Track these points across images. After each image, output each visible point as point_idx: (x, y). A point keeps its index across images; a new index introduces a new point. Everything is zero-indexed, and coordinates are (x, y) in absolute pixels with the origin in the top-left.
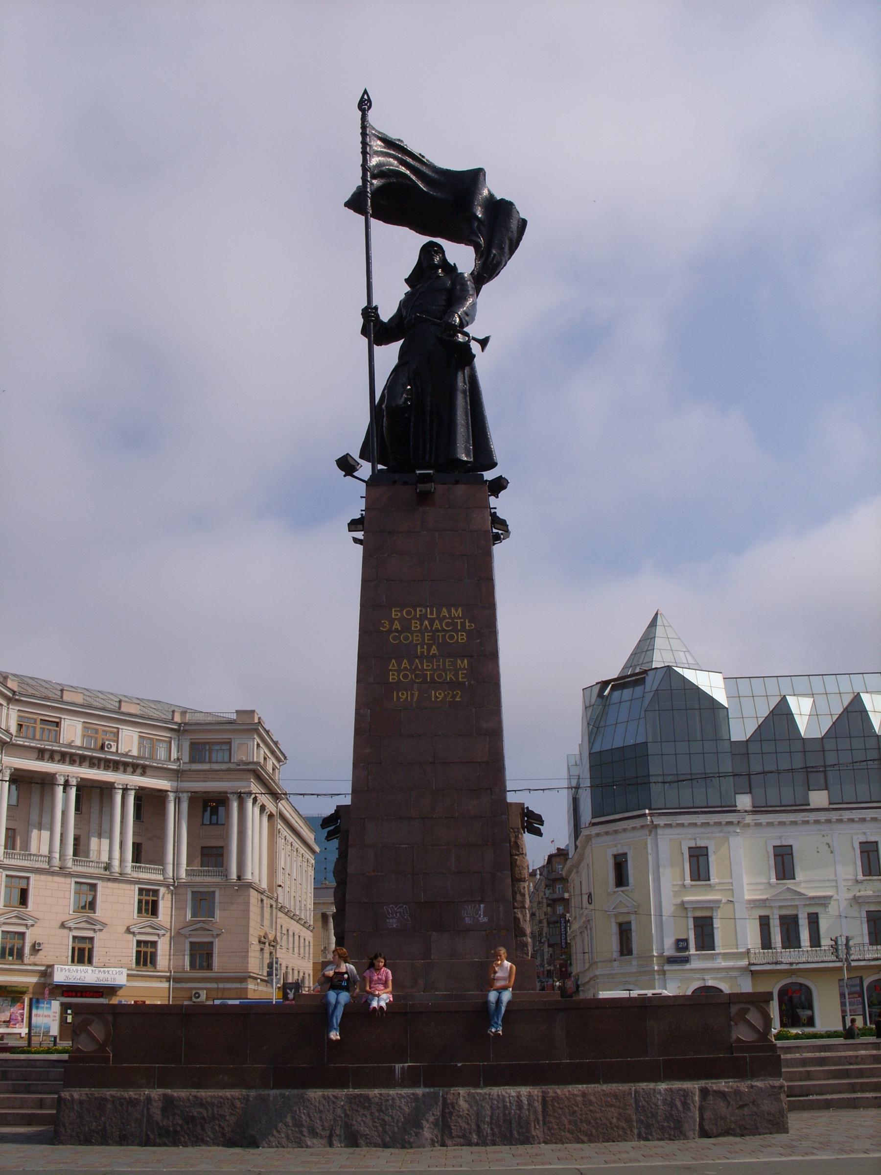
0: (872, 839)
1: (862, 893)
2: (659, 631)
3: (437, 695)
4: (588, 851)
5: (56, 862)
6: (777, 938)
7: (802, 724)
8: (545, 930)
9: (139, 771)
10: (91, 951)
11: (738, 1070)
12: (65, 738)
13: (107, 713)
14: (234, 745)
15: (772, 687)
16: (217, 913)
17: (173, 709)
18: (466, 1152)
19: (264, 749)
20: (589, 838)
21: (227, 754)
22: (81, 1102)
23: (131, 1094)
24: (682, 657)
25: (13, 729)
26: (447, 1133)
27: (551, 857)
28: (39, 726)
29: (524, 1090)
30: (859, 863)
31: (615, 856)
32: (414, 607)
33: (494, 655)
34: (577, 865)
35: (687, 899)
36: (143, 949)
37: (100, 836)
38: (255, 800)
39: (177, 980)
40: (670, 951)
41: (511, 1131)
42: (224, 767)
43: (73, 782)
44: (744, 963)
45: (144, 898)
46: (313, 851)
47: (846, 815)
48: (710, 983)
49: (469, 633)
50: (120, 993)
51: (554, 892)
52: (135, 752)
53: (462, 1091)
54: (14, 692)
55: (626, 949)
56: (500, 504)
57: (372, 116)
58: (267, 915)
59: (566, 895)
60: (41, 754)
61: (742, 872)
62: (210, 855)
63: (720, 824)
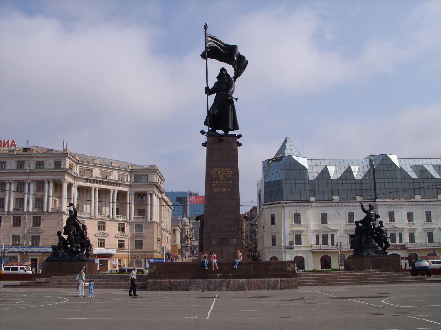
0: (352, 212)
1: (348, 228)
2: (288, 143)
3: (224, 190)
4: (263, 212)
5: (93, 215)
6: (321, 242)
8: (249, 235)
9: (118, 185)
10: (104, 243)
11: (288, 276)
12: (94, 175)
13: (108, 166)
14: (149, 176)
15: (323, 163)
16: (144, 231)
17: (129, 164)
18: (232, 292)
19: (158, 177)
20: (263, 209)
21: (146, 179)
22: (152, 282)
23: (162, 280)
24: (295, 152)
25: (78, 173)
26: (228, 288)
27: (251, 210)
28: (86, 171)
29: (244, 280)
30: (347, 219)
31: (271, 215)
32: (219, 168)
33: (238, 180)
34: (260, 216)
35: (293, 229)
36: (120, 243)
37: (105, 206)
38: (156, 194)
39: (131, 252)
40: (287, 245)
41: (241, 288)
42: (145, 184)
44: (311, 249)
45: (120, 226)
46: (171, 209)
47: (344, 204)
48: (300, 255)
49: (232, 174)
50: (113, 256)
51: (252, 222)
52: (117, 179)
53: (231, 280)
54: (78, 161)
55: (274, 244)
56: (240, 140)
57: (208, 31)
58: (159, 231)
59: (256, 223)
60: (87, 180)
61: (311, 221)
62: (141, 212)
63: (304, 206)
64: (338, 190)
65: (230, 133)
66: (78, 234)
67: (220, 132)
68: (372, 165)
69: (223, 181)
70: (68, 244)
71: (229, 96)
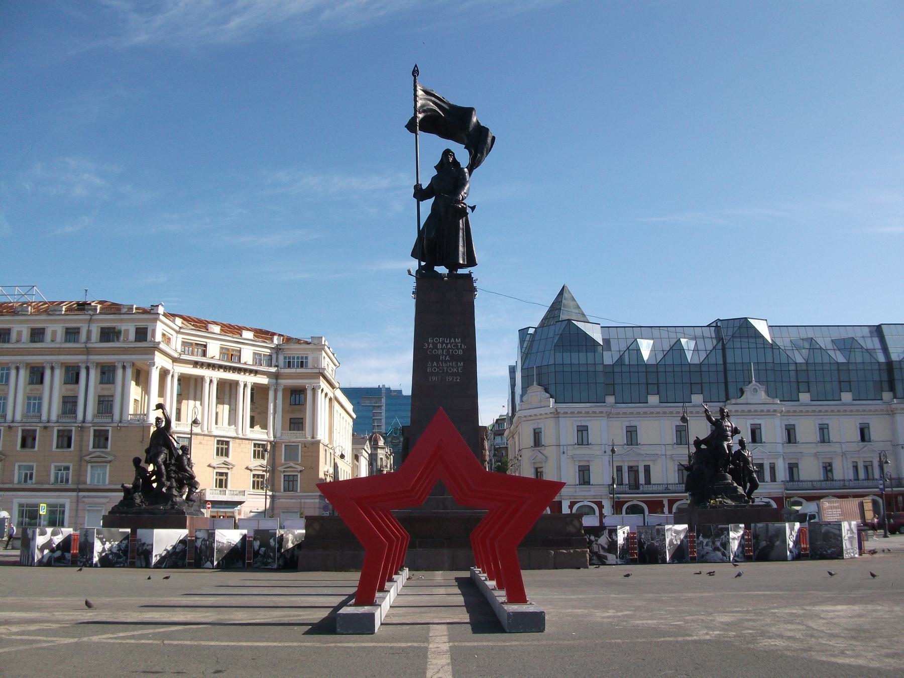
7: (646, 354)
60: (196, 364)
64: (658, 384)
65: (460, 271)
66: (173, 462)
67: (442, 270)
68: (719, 338)
70: (154, 481)
71: (459, 202)
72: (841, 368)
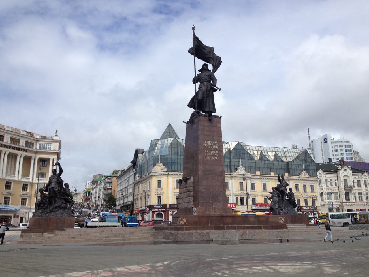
32: (209, 141)
43: (7, 153)
69: (212, 151)
72: (271, 163)
